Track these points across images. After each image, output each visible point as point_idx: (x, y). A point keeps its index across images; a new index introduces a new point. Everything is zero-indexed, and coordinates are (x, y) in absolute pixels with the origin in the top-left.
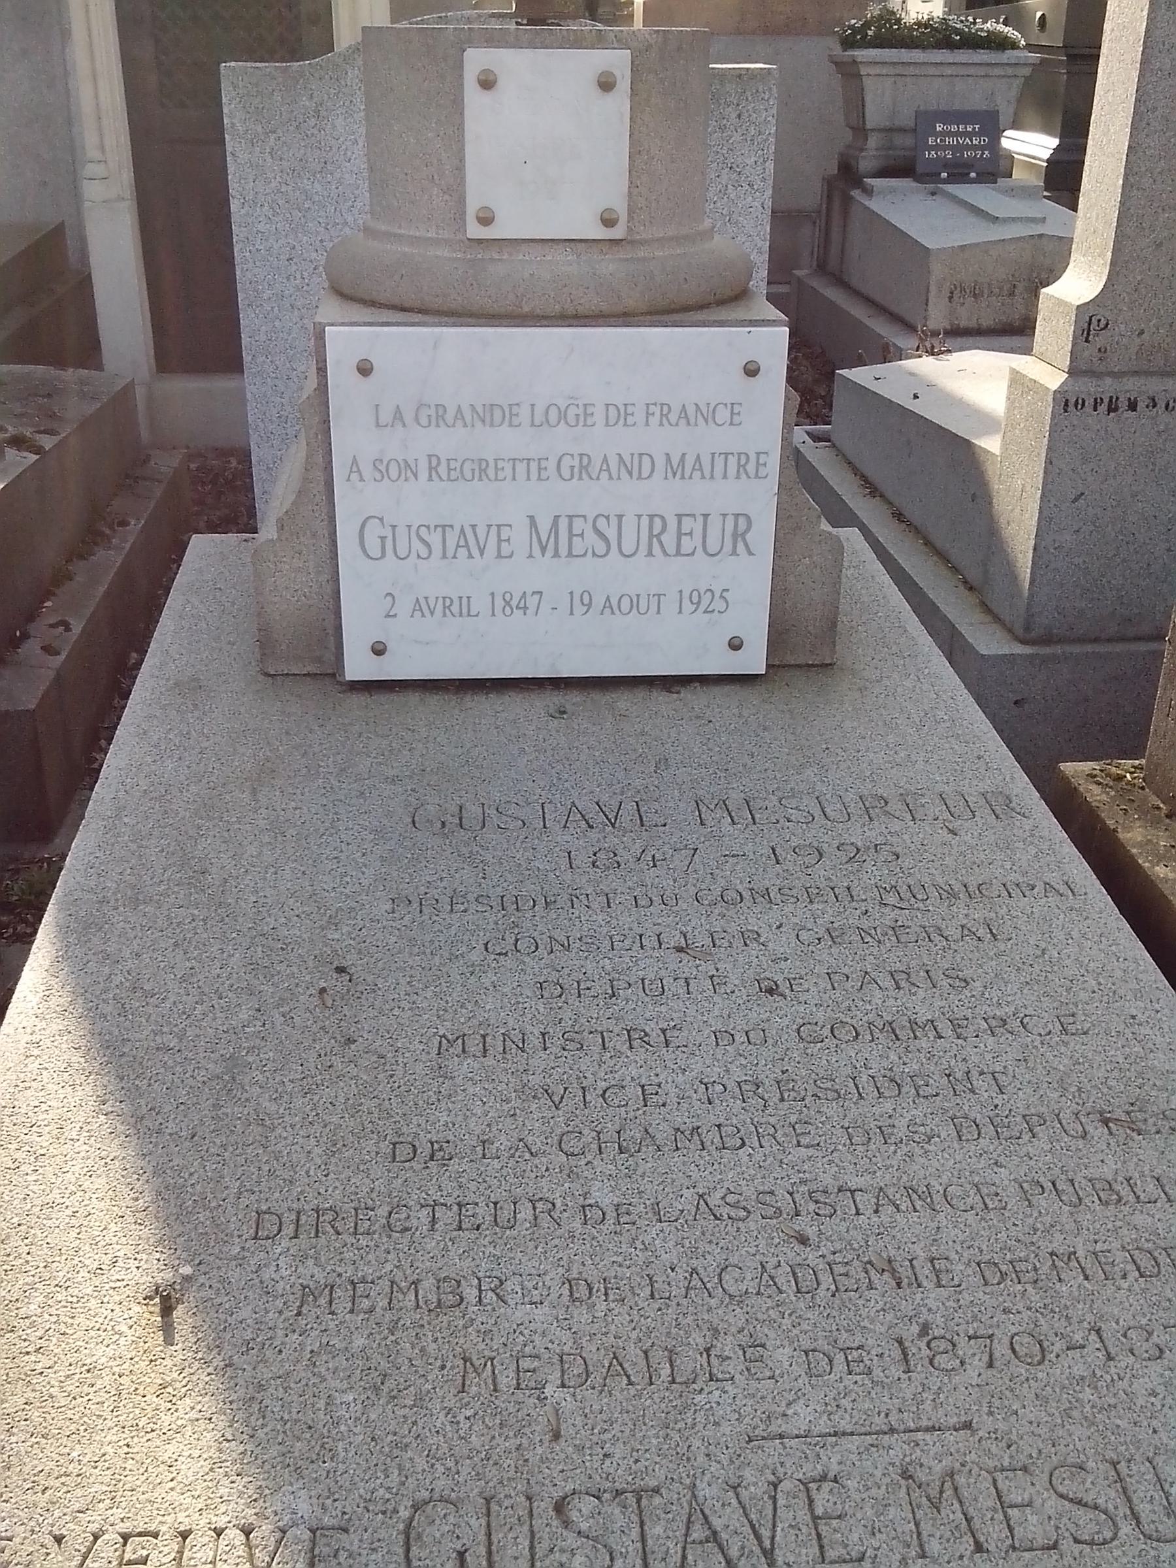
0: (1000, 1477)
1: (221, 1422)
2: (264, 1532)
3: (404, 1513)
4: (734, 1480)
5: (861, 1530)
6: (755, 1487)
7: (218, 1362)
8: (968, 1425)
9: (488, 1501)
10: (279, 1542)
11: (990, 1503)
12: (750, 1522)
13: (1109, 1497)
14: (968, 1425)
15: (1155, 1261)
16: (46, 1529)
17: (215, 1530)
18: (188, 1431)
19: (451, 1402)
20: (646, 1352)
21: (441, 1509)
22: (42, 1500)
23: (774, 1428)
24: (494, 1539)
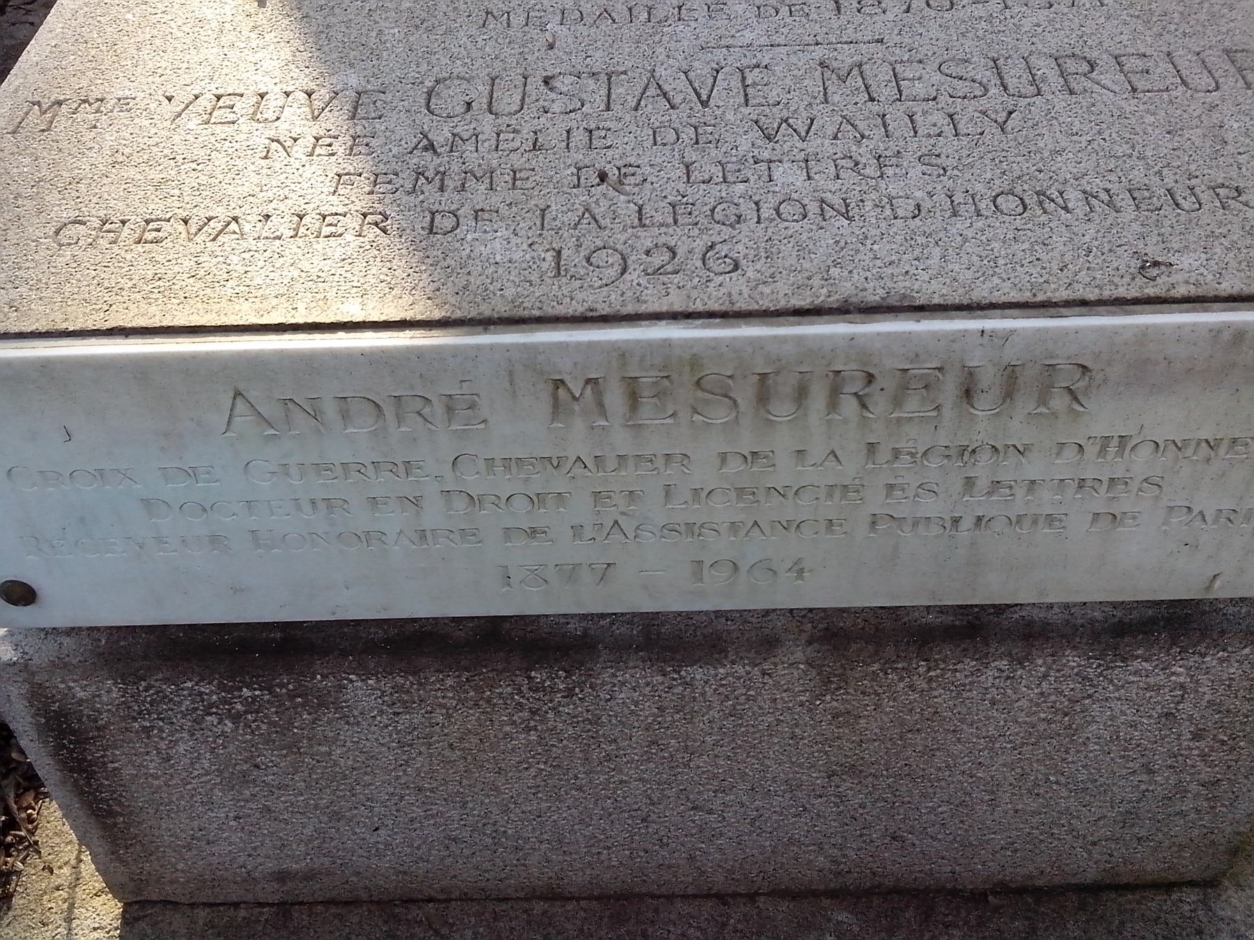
0: (898, 66)
1: (297, 43)
2: (323, 94)
3: (428, 84)
4: (685, 67)
5: (779, 90)
6: (701, 69)
7: (299, 15)
8: (881, 41)
9: (493, 80)
10: (332, 99)
11: (887, 78)
12: (695, 90)
13: (988, 75)
14: (881, 41)
15: (1230, 361)
16: (161, 92)
17: (298, 216)
18: (272, 47)
19: (473, 31)
20: (630, 9)
21: (457, 82)
22: (158, 80)
23: (723, 43)
24: (495, 95)
